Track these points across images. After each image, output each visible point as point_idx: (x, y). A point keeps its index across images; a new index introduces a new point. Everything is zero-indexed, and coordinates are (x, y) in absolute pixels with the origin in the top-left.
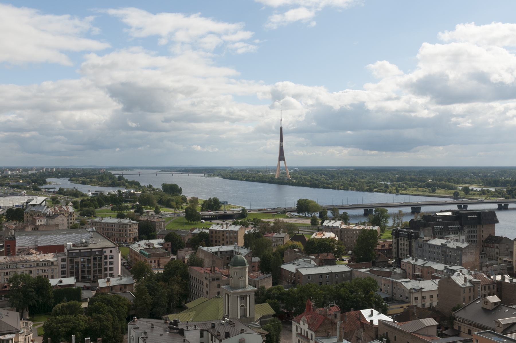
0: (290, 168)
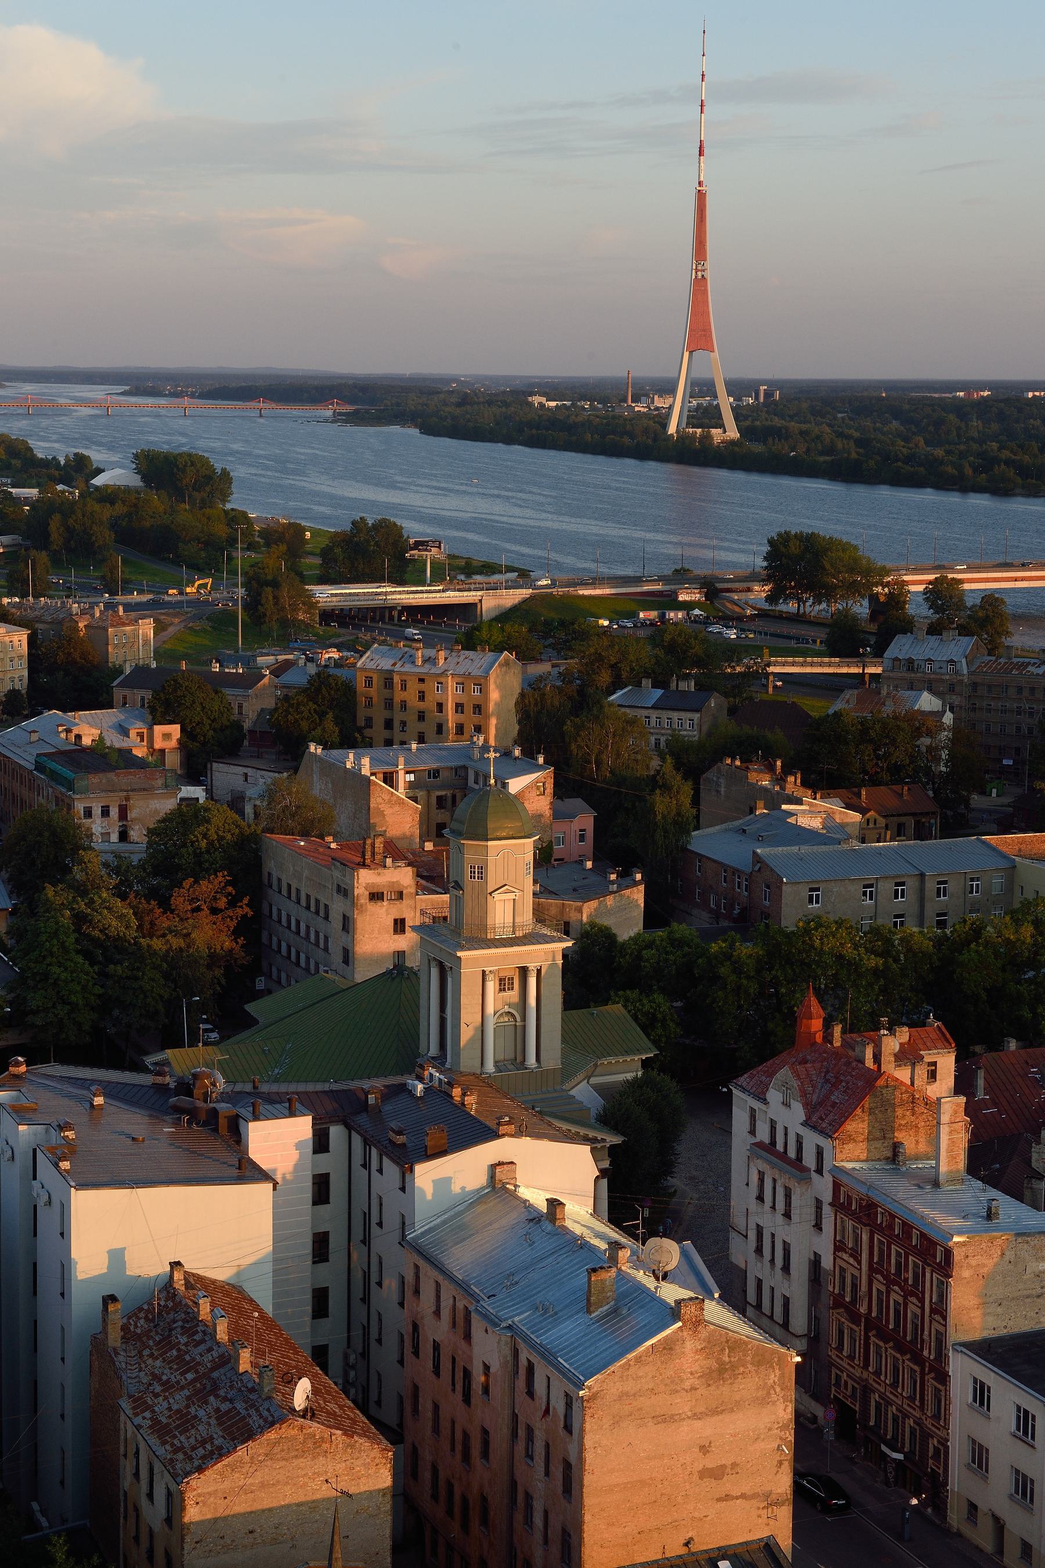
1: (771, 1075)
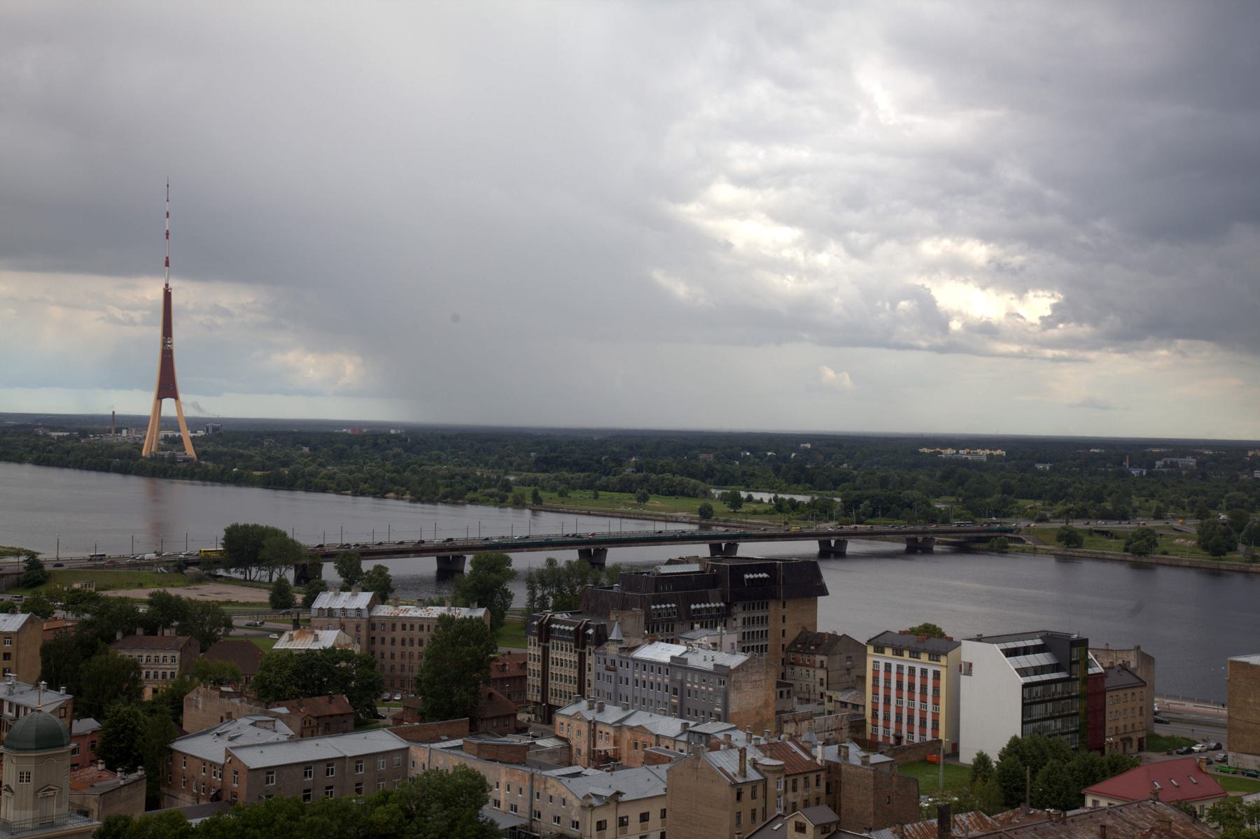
0: (194, 424)
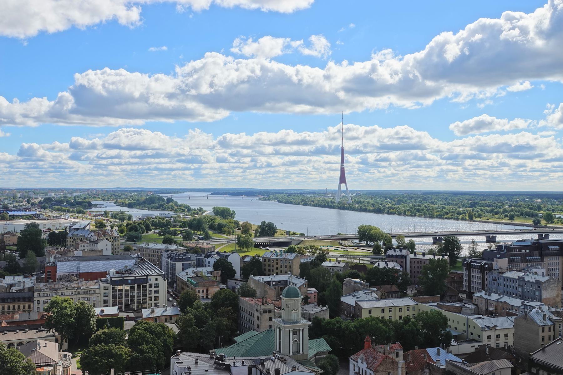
0: (352, 192)
1: (359, 355)
